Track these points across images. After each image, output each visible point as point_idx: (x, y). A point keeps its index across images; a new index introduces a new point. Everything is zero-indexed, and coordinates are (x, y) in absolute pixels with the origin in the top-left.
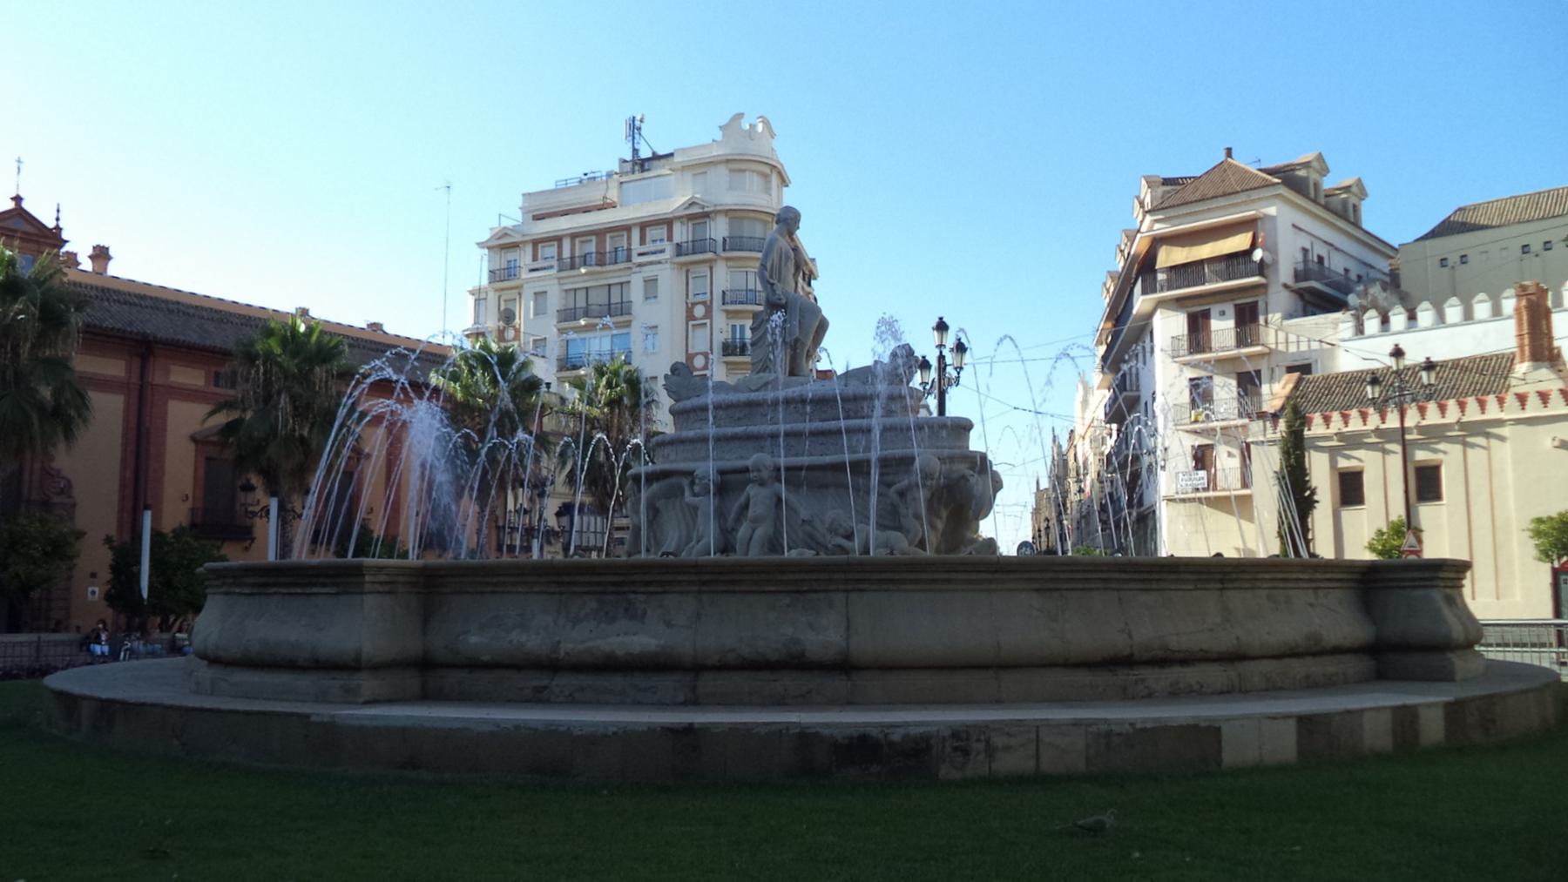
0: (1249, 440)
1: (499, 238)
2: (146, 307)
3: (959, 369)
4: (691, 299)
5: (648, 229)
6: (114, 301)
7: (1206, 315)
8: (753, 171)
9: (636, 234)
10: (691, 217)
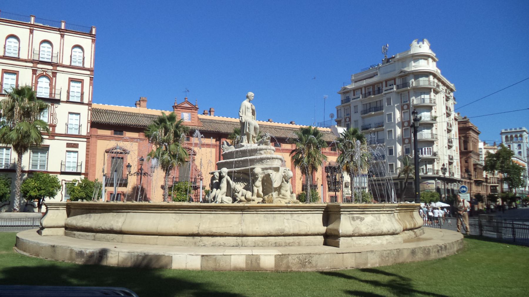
1: (343, 90)
4: (403, 104)
5: (388, 82)
9: (384, 84)
10: (401, 77)
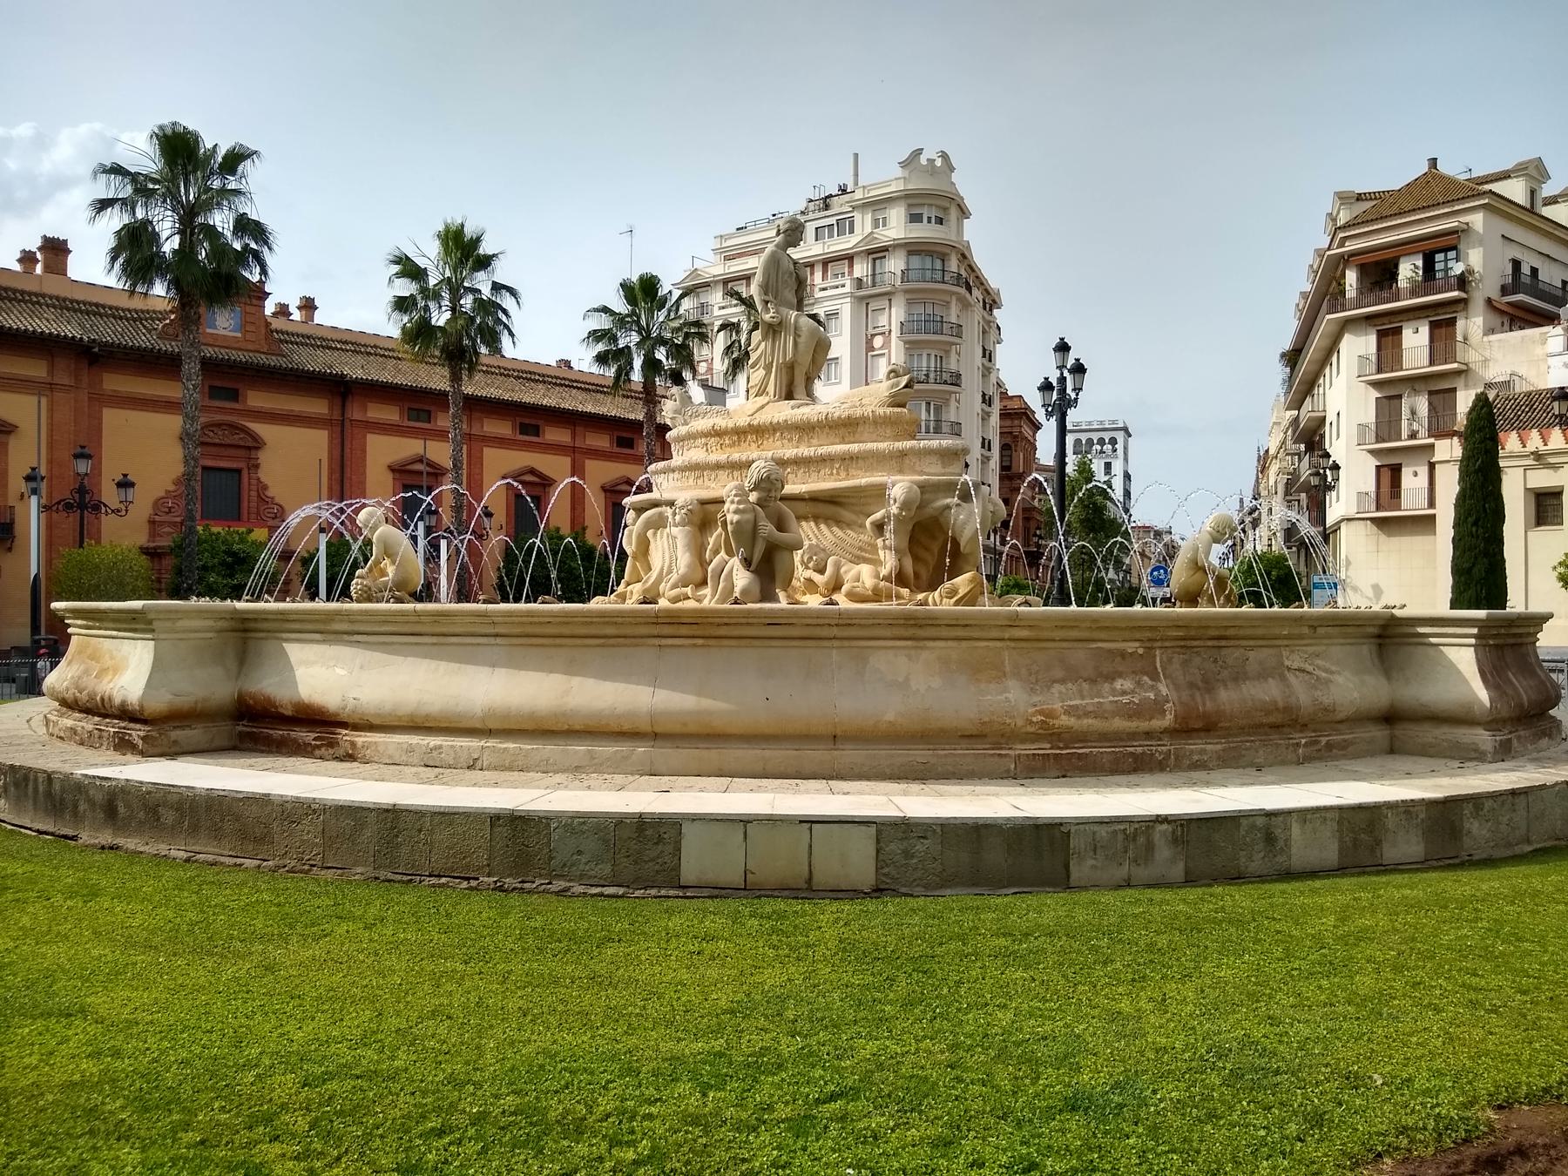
0: (1434, 460)
2: (347, 351)
3: (1078, 390)
4: (871, 331)
6: (318, 347)
7: (1398, 332)
8: (931, 205)
10: (869, 252)
